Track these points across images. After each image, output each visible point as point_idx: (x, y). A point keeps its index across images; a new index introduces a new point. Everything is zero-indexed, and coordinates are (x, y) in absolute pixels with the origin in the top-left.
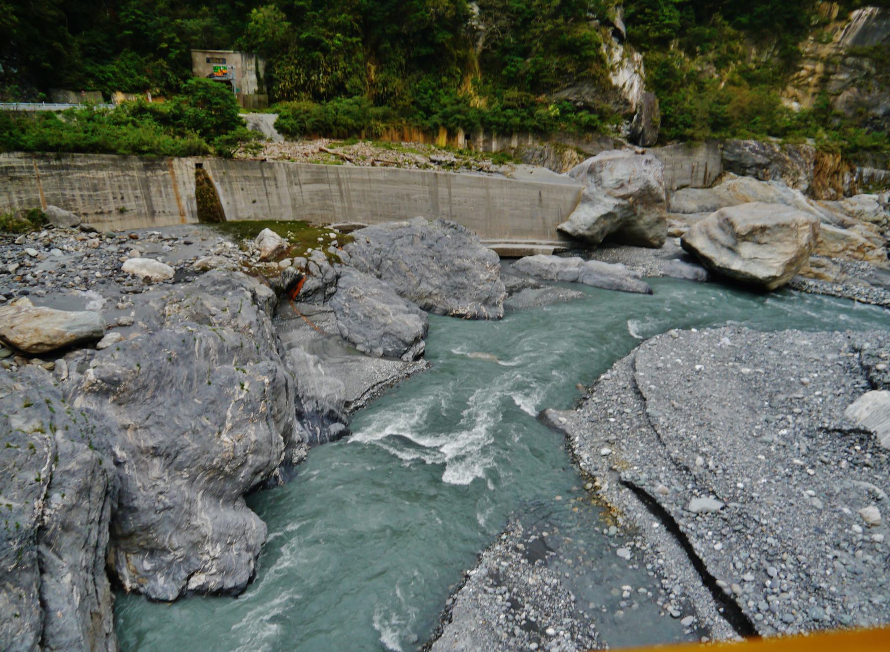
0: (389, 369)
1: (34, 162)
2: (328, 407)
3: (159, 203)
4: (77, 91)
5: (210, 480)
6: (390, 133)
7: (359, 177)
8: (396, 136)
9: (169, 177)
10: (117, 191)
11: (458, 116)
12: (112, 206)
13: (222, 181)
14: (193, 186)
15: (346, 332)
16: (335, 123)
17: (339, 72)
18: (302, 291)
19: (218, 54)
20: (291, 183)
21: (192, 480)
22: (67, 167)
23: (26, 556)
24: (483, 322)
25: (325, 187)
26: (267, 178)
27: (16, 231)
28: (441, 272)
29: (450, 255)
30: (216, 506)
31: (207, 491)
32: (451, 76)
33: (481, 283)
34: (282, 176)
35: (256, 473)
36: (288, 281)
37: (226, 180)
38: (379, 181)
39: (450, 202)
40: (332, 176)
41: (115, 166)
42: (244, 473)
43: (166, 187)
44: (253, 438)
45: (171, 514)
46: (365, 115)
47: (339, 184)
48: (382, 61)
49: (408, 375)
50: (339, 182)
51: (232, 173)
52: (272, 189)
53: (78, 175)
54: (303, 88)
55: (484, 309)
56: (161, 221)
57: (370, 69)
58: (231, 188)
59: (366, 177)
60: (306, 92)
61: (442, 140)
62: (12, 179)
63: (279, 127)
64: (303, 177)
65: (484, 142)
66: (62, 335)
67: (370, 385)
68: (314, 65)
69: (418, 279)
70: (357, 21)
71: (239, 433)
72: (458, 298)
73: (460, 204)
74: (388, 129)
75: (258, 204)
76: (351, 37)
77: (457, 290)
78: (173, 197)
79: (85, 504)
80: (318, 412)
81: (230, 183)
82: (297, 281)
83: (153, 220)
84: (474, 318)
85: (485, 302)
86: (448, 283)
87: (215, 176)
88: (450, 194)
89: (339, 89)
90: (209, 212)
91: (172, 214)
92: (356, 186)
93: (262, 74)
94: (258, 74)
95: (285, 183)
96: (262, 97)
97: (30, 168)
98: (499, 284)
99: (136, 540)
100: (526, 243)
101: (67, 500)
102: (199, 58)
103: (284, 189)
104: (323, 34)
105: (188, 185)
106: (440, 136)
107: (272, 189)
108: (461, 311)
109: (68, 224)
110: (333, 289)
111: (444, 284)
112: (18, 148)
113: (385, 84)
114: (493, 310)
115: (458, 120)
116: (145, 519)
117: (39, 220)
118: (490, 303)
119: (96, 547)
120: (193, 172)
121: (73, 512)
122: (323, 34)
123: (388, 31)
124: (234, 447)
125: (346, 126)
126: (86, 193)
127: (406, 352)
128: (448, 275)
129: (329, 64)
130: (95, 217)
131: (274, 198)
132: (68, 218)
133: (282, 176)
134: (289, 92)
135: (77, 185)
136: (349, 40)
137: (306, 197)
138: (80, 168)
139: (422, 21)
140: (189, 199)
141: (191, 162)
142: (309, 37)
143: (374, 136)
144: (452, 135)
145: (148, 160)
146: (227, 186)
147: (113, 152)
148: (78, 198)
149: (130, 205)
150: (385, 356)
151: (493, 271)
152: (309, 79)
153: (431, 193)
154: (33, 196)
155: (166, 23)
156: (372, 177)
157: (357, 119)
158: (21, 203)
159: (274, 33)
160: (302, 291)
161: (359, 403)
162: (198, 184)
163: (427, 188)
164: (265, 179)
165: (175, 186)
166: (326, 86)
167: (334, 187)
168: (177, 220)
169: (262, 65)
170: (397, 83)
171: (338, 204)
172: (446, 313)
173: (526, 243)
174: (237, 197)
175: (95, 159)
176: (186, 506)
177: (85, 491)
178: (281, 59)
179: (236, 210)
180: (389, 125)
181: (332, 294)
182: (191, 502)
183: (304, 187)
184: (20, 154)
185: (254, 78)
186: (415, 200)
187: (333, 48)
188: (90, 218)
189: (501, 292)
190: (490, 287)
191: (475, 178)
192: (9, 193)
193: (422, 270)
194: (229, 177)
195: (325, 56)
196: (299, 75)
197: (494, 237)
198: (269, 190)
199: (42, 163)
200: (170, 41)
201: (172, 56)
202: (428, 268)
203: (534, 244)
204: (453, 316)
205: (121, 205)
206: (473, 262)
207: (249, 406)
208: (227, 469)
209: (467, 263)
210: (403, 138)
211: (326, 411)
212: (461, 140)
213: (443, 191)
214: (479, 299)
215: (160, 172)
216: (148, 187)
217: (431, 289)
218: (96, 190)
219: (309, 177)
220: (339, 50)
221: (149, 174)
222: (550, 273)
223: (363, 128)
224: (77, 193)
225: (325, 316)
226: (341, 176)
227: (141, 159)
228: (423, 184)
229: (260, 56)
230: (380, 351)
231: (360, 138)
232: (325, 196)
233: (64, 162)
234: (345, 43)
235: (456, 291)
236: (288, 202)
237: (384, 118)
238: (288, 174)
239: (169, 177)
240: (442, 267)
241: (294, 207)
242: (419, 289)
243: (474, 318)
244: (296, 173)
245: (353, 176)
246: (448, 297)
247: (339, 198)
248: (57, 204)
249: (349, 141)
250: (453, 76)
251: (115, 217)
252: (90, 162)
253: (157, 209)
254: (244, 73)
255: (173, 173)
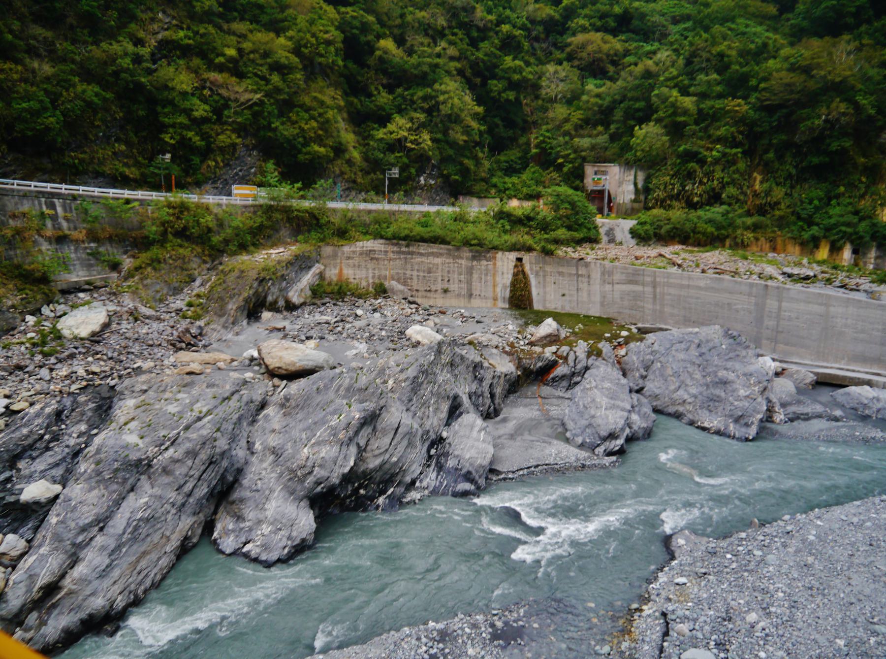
0: (570, 454)
1: (390, 248)
2: (467, 467)
3: (477, 287)
4: (480, 197)
5: (290, 479)
6: (760, 243)
7: (679, 281)
8: (767, 246)
9: (491, 267)
10: (446, 274)
11: (843, 228)
12: (439, 286)
13: (537, 274)
14: (510, 277)
15: (566, 419)
16: (694, 232)
17: (716, 182)
18: (551, 376)
19: (603, 167)
20: (604, 282)
21: (281, 475)
22: (412, 253)
23: (121, 475)
24: (727, 440)
25: (639, 288)
26: (581, 275)
27: (360, 297)
28: (702, 381)
29: (716, 366)
30: (286, 500)
31: (285, 487)
32: (851, 186)
33: (738, 399)
34: (596, 275)
35: (318, 483)
36: (540, 364)
37: (541, 273)
38: (699, 288)
39: (778, 317)
40: (648, 279)
41: (449, 254)
42: (310, 480)
43: (486, 275)
44: (322, 455)
45: (257, 495)
46: (731, 224)
47: (654, 287)
48: (768, 170)
49: (584, 466)
50: (654, 285)
51: (548, 268)
52: (584, 286)
53: (419, 259)
54: (677, 197)
55: (732, 427)
56: (476, 302)
57: (755, 179)
58: (544, 281)
59: (685, 282)
60: (679, 201)
61: (823, 253)
62: (372, 259)
63: (633, 233)
64: (617, 277)
65: (877, 258)
66: (294, 364)
67: (535, 464)
68: (690, 175)
69: (677, 384)
70: (741, 133)
71: (316, 449)
72: (710, 411)
73: (790, 319)
74: (757, 239)
75: (567, 298)
76: (732, 148)
77: (711, 403)
78: (490, 284)
79: (189, 463)
80: (456, 469)
81: (544, 276)
82: (552, 365)
83: (469, 301)
84: (718, 433)
85: (737, 420)
86: (705, 394)
87: (531, 269)
88: (780, 308)
89: (714, 198)
90: (520, 300)
91: (486, 298)
92: (672, 291)
93: (640, 186)
94: (635, 184)
95: (598, 281)
96: (636, 205)
97: (386, 252)
98: (759, 404)
99: (234, 506)
100: (867, 373)
101: (178, 455)
102: (589, 170)
103: (596, 287)
104: (703, 147)
105: (505, 276)
106: (821, 250)
107: (584, 286)
108: (706, 425)
109: (401, 296)
110: (579, 379)
111: (701, 393)
112: (382, 237)
113: (768, 193)
114: (744, 430)
115: (845, 232)
116: (248, 494)
117: (381, 291)
118: (742, 422)
119: (189, 495)
120: (512, 264)
121: (177, 465)
122: (703, 147)
123: (774, 141)
124: (308, 458)
125: (704, 234)
126: (422, 274)
127: (599, 445)
128: (707, 386)
129: (707, 174)
130: (424, 294)
131: (584, 295)
132: (402, 292)
133: (596, 275)
134: (663, 201)
135: (416, 267)
136: (728, 150)
137: (617, 295)
138: (421, 255)
139: (812, 129)
140: (504, 287)
141: (513, 256)
142: (685, 150)
143: (739, 245)
144: (835, 249)
145: (477, 251)
146: (541, 279)
147: (448, 243)
148: (415, 278)
149: (454, 287)
150: (582, 446)
151: (756, 388)
152: (684, 189)
153: (756, 304)
154: (383, 273)
155: (566, 143)
156: (691, 283)
157: (719, 228)
158: (373, 277)
159: (651, 147)
160: (551, 376)
161: (510, 476)
162: (515, 275)
163: (753, 300)
164: (578, 275)
165: (494, 275)
166: (701, 196)
167: (648, 289)
168: (490, 303)
169: (641, 176)
170: (779, 193)
171: (649, 306)
172: (692, 423)
173: (867, 373)
174: (548, 289)
175: (435, 248)
176: (267, 492)
177: (192, 454)
178: (659, 170)
179: (545, 300)
180: (759, 235)
181: (577, 383)
182: (272, 491)
183: (617, 287)
184: (382, 241)
185: (631, 187)
186: (737, 311)
187: (709, 159)
188: (420, 294)
189: (759, 413)
190: (747, 404)
191: (814, 294)
192: (367, 269)
193: (684, 377)
194: (544, 271)
195: (701, 167)
196: (673, 185)
197: (827, 361)
198: (581, 286)
199: (395, 249)
200: (566, 157)
201: (565, 169)
202: (691, 375)
203: (878, 375)
204: (698, 427)
205: (446, 286)
206: (738, 377)
207: (334, 432)
208: (299, 473)
209: (731, 376)
210: (774, 249)
211: (464, 471)
212: (847, 254)
213: (772, 304)
214: (731, 416)
215: (484, 263)
216: (471, 274)
217: (686, 397)
218: (429, 272)
219: (623, 277)
220: (717, 161)
221: (475, 263)
222: (870, 408)
223: (727, 237)
224: (415, 273)
225: (560, 401)
226: (658, 280)
227: (471, 251)
228: (750, 294)
229: (642, 168)
230: (579, 440)
231: (724, 246)
232: (637, 297)
233: (411, 249)
234: (724, 155)
235: (711, 403)
236: (597, 298)
237: (755, 227)
238: (603, 274)
239: (491, 267)
240: (704, 376)
241: (602, 304)
242: (675, 396)
243: (718, 433)
244: (611, 273)
245: (671, 281)
246: (701, 407)
247: (651, 300)
248: (398, 281)
249: (708, 248)
250: (856, 187)
251: (439, 295)
252: (430, 250)
253: (474, 293)
254: (620, 184)
255: (495, 264)
